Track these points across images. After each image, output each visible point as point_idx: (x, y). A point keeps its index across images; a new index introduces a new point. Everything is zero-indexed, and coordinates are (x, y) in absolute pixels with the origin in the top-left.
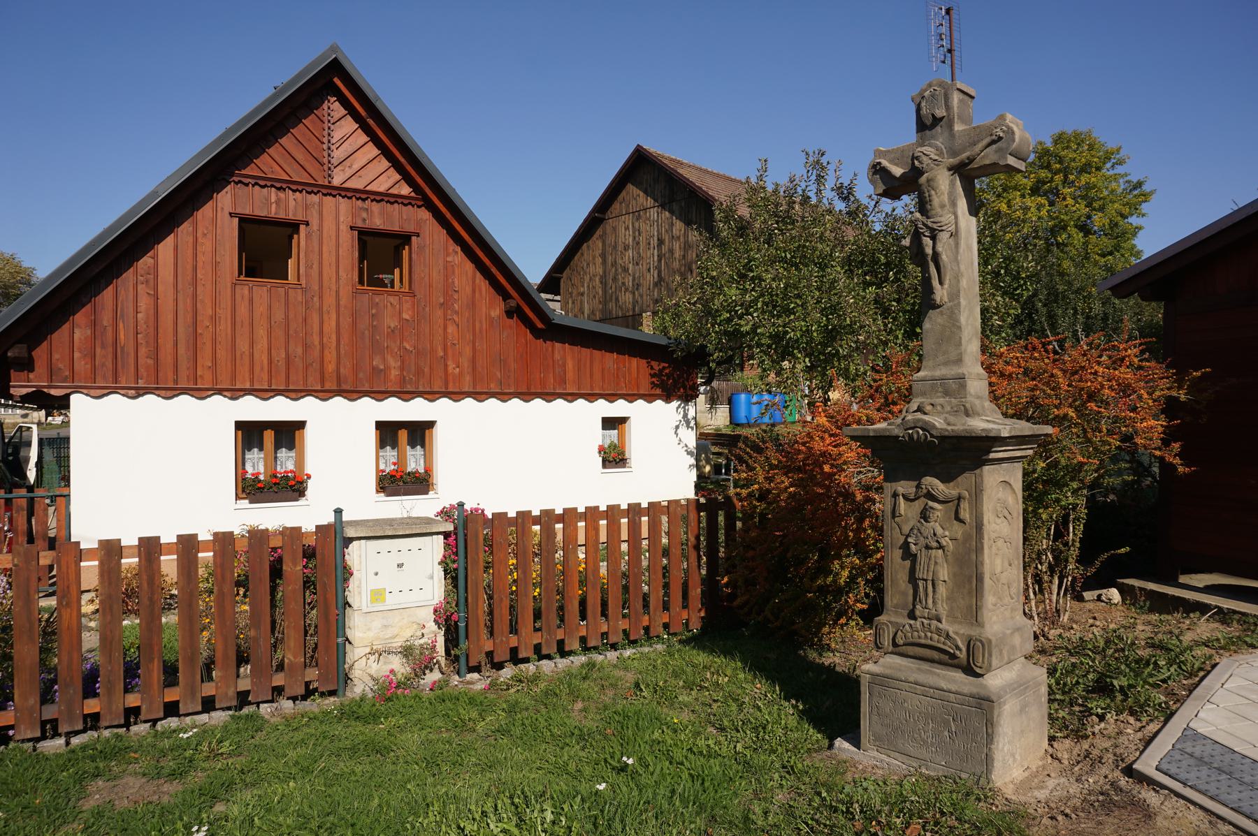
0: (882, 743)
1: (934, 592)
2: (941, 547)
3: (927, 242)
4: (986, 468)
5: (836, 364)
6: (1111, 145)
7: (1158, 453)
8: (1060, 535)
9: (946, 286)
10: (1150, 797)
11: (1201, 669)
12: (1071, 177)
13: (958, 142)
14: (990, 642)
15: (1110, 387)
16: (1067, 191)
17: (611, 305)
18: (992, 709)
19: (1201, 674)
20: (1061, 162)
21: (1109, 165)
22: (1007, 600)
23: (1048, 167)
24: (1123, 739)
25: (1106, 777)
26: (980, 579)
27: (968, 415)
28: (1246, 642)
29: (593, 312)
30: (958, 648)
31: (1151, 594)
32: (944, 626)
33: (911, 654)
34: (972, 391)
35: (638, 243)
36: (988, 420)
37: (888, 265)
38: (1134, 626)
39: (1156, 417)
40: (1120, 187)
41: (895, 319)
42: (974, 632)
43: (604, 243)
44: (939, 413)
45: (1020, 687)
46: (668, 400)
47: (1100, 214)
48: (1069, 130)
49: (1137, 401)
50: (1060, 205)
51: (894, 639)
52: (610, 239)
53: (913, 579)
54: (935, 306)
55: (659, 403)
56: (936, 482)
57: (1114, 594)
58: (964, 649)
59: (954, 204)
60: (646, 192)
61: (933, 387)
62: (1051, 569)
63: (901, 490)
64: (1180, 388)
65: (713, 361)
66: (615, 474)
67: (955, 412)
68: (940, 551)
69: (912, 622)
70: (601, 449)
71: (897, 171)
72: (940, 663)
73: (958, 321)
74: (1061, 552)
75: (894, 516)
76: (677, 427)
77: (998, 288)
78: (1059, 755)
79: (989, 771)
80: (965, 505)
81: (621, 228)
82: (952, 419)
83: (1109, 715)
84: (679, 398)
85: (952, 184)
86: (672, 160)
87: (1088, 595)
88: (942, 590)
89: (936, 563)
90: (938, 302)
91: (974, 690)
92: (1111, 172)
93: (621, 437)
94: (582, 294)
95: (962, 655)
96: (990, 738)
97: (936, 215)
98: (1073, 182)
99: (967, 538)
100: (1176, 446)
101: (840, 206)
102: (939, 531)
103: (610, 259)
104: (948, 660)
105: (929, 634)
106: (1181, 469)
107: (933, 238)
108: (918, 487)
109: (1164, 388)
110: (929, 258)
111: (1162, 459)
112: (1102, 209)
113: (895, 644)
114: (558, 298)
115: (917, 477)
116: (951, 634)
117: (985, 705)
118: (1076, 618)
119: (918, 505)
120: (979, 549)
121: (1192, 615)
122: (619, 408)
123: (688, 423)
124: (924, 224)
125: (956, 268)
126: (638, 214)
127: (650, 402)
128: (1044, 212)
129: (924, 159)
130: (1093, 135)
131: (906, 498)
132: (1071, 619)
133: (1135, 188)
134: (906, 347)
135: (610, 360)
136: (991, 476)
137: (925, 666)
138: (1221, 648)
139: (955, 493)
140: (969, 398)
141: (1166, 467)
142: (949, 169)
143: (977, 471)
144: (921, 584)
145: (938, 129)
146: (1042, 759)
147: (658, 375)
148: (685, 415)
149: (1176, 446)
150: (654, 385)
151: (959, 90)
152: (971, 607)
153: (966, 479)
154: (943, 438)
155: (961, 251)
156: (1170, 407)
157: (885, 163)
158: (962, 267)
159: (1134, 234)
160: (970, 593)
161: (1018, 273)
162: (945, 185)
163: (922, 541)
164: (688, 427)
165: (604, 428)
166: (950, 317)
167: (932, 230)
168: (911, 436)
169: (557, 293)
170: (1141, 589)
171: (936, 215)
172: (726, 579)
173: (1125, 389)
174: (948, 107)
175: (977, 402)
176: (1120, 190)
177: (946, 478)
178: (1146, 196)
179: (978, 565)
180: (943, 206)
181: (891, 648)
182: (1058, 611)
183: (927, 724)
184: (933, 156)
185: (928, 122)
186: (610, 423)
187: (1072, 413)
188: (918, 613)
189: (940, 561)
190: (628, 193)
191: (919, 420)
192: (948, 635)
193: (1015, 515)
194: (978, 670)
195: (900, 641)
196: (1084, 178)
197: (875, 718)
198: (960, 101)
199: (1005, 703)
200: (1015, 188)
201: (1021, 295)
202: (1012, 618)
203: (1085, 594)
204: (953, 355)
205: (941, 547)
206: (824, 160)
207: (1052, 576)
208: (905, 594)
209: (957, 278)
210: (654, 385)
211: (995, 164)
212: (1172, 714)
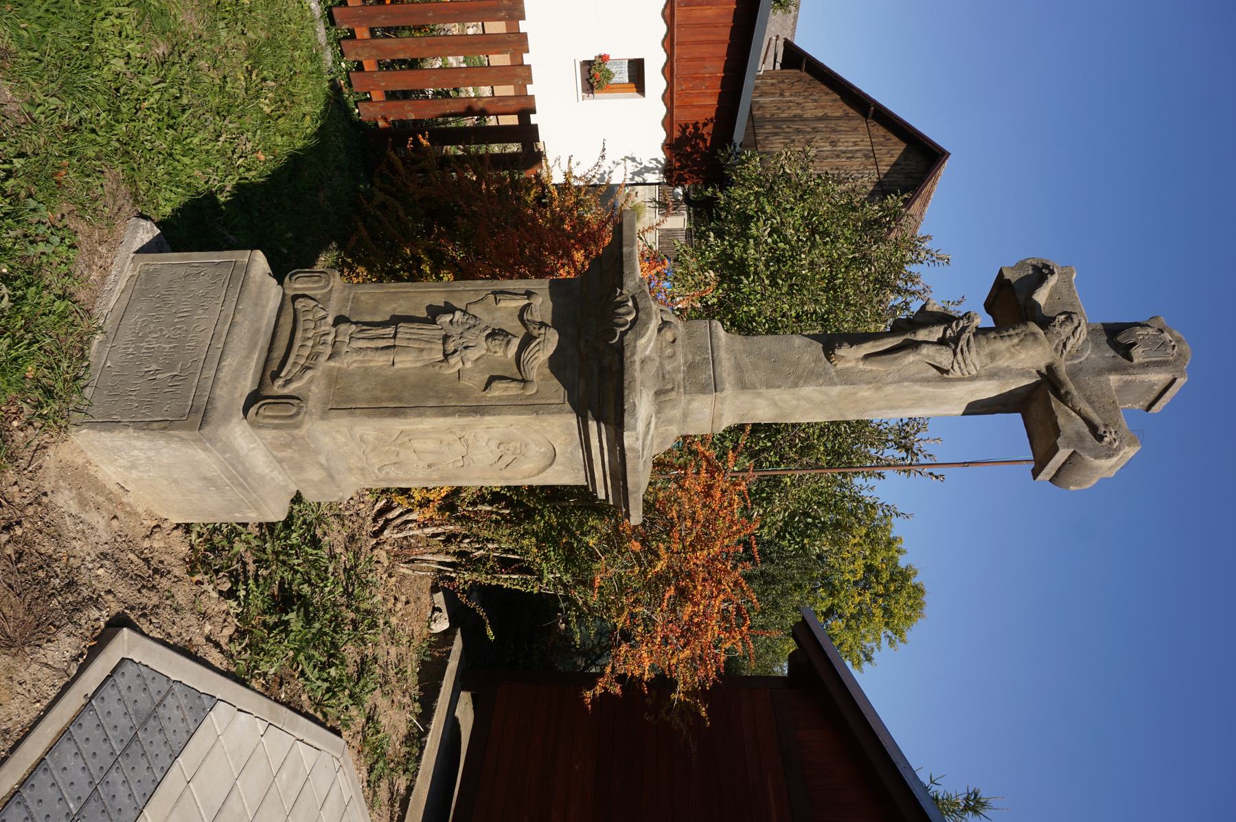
0: (142, 286)
1: (377, 349)
2: (446, 356)
3: (937, 333)
4: (573, 420)
6: (908, 635)
7: (608, 670)
8: (506, 564)
9: (861, 366)
10: (63, 648)
11: (325, 715)
12: (880, 600)
13: (1091, 381)
14: (298, 426)
15: (695, 614)
16: (868, 597)
17: (769, 128)
18: (190, 427)
19: (319, 715)
20: (896, 591)
21: (889, 633)
22: (376, 461)
23: (892, 580)
24: (191, 619)
25: (109, 592)
26: (397, 412)
27: (658, 394)
28: (377, 762)
29: (761, 107)
30: (288, 382)
31: (444, 664)
32: (323, 363)
33: (282, 321)
34: (695, 405)
35: (838, 156)
36: (649, 429)
38: (395, 642)
39: (652, 668)
40: (868, 643)
42: (312, 404)
43: (838, 118)
44: (661, 351)
45: (241, 476)
46: (668, 146)
47: (843, 626)
48: (926, 598)
49: (672, 644)
50: (853, 590)
51: (304, 296)
52: (843, 125)
53: (396, 320)
54: (829, 351)
55: (662, 135)
56: (551, 348)
57: (442, 625)
58: (286, 391)
59: (992, 375)
60: (896, 164)
61: (702, 348)
62: (462, 554)
63: (537, 301)
64: (686, 693)
65: (714, 193)
66: (574, 79)
67: (662, 375)
68: (440, 356)
69: (330, 320)
70: (604, 58)
71: (1041, 296)
72: (268, 360)
73: (806, 383)
74: (484, 565)
75: (495, 293)
76: (633, 160)
77: (792, 515)
78: (157, 536)
79: (93, 425)
80: (513, 389)
81: (856, 137)
82: (652, 368)
83: (234, 604)
84: (668, 161)
85: (1024, 373)
86: (930, 193)
87: (439, 598)
88: (380, 360)
89: (421, 350)
90: (840, 352)
91: (220, 405)
92: (882, 635)
93: (620, 88)
94: (782, 95)
95: (277, 388)
96: (144, 426)
98: (875, 602)
99: (462, 394)
100: (617, 689)
102: (472, 355)
103: (821, 125)
104: (270, 371)
105: (310, 343)
106: (589, 694)
107: (942, 342)
108: (542, 324)
109: (685, 680)
110: (909, 336)
111: (602, 674)
112: (848, 627)
113: (295, 298)
114: (778, 66)
115: (558, 322)
116: (309, 374)
117: (197, 417)
118: (407, 583)
119: (514, 326)
120: (443, 410)
121: (417, 705)
122: (655, 82)
123: (639, 173)
124: (964, 329)
125: (890, 378)
126: (871, 155)
127: (664, 123)
128: (848, 576)
129: (1069, 328)
131: (524, 309)
132: (404, 576)
133: (866, 655)
135: (715, 69)
136: (560, 428)
137: (263, 341)
138: (365, 737)
139: (533, 374)
140: (684, 399)
141: (591, 681)
142: (1050, 368)
143: (568, 406)
144: (390, 331)
145: (1111, 353)
146: (150, 515)
147: (697, 135)
148: (647, 170)
149: (617, 689)
150: (684, 128)
151: (1174, 380)
152: (354, 401)
153: (556, 391)
154: (620, 350)
155: (917, 387)
156: (663, 682)
157: (1053, 281)
158: (890, 389)
160: (376, 399)
161: (808, 536)
162: (1023, 359)
163: (455, 331)
164: (634, 174)
165: (630, 61)
166: (812, 372)
167: (956, 340)
168: (623, 304)
169: (783, 66)
170: (449, 653)
171: (979, 346)
172: (425, 142)
173: (690, 632)
174: (1146, 366)
175: (677, 413)
176: (864, 643)
177: (556, 364)
179: (418, 409)
180: (992, 356)
181: (290, 293)
182: (412, 561)
183: (169, 340)
184: (1072, 341)
185: (1122, 338)
186: (637, 68)
187: (660, 566)
188: (343, 327)
189: (425, 356)
190: (895, 144)
191: (649, 315)
192: (308, 368)
193: (506, 473)
194: (253, 410)
195: (300, 304)
196: (879, 612)
197: (182, 271)
198: (1151, 386)
199: (205, 450)
200: (873, 551)
201: (784, 538)
202: (350, 469)
203: (440, 594)
204: (750, 377)
205: (446, 356)
207: (455, 553)
208: (375, 310)
209: (875, 381)
210: (684, 128)
211: (1057, 432)
212: (243, 683)
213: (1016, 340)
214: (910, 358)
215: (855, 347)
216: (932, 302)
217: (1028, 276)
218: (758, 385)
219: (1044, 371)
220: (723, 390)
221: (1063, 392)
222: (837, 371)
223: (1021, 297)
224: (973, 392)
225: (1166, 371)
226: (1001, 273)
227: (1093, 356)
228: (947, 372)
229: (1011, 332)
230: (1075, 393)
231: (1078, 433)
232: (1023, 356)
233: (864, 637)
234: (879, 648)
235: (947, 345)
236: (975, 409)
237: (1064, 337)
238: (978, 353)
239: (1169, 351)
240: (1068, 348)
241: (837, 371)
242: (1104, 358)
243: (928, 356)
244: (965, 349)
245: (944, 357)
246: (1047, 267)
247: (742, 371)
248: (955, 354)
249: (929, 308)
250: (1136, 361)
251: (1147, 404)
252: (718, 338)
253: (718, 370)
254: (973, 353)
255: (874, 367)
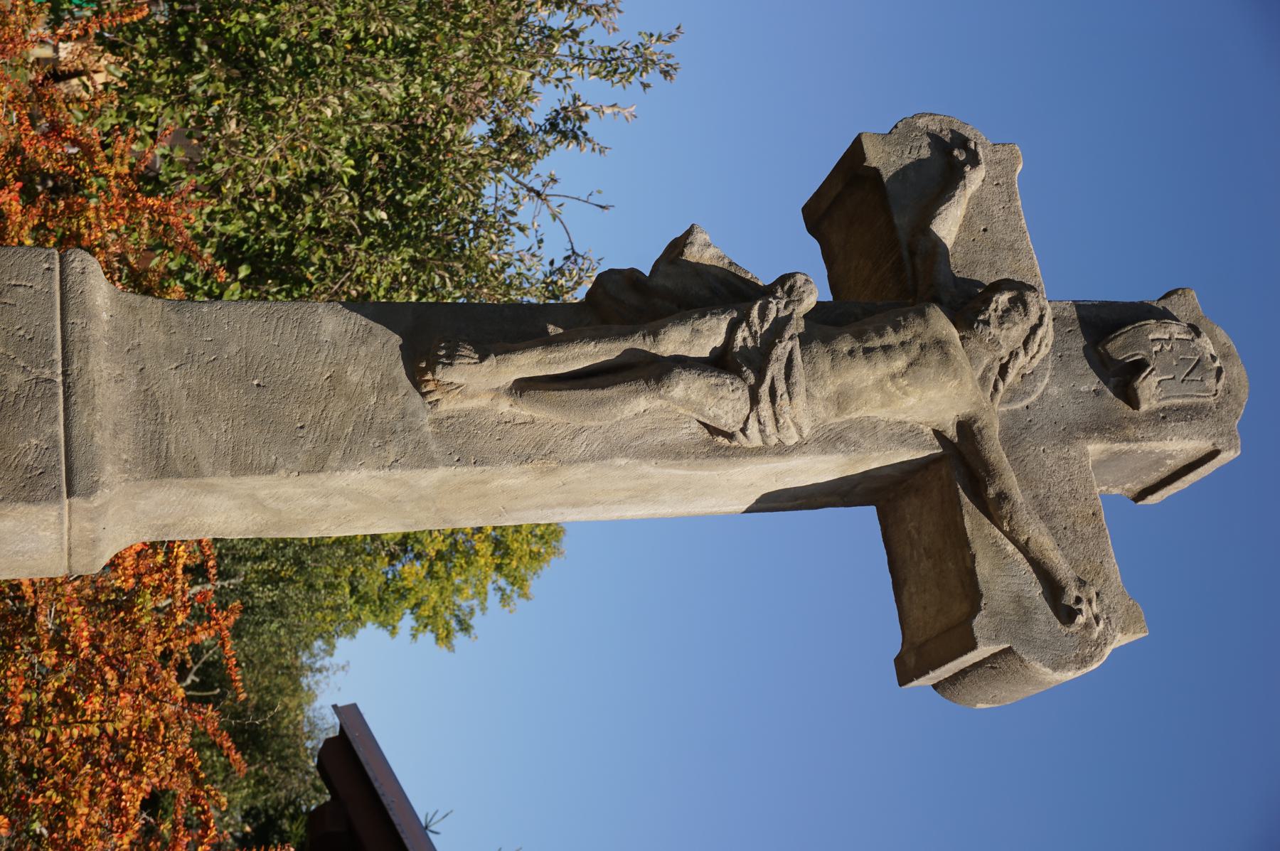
3: (706, 336)
5: (164, 63)
6: (533, 585)
9: (505, 406)
21: (502, 582)
37: (398, 210)
41: (274, 219)
47: (423, 573)
59: (830, 440)
73: (350, 458)
90: (445, 375)
92: (490, 587)
97: (813, 376)
101: (539, 112)
107: (721, 362)
110: (638, 342)
112: (431, 574)
124: (780, 325)
129: (1018, 331)
130: (554, 559)
134: (201, 239)
142: (965, 426)
145: (1091, 382)
151: (1213, 454)
157: (975, 179)
158: (578, 473)
159: (383, 625)
167: (758, 359)
171: (813, 376)
174: (1162, 417)
176: (459, 600)
178: (445, 638)
180: (841, 401)
185: (1119, 348)
204: (185, 436)
206: (653, 76)
211: (973, 596)
213: (900, 363)
214: (636, 407)
215: (492, 361)
216: (700, 237)
217: (919, 163)
218: (206, 465)
219: (951, 433)
220: (91, 491)
221: (992, 492)
222: (438, 422)
223: (902, 221)
224: (779, 475)
225: (1201, 434)
226: (856, 151)
227: (1054, 391)
228: (730, 436)
229: (891, 338)
230: (1018, 495)
231: (1018, 599)
232: (912, 401)
233: (458, 590)
234: (484, 609)
235: (737, 372)
236: (771, 503)
237: (1004, 353)
238: (809, 395)
239: (1210, 382)
240: (1012, 376)
241: (438, 422)
242: (1077, 395)
243: (686, 402)
244: (781, 387)
245: (727, 406)
246: (962, 142)
247: (159, 419)
248: (755, 400)
249: (693, 254)
250: (1144, 407)
251: (1139, 487)
252: (89, 315)
253: (82, 420)
254: (800, 400)
255: (539, 413)
